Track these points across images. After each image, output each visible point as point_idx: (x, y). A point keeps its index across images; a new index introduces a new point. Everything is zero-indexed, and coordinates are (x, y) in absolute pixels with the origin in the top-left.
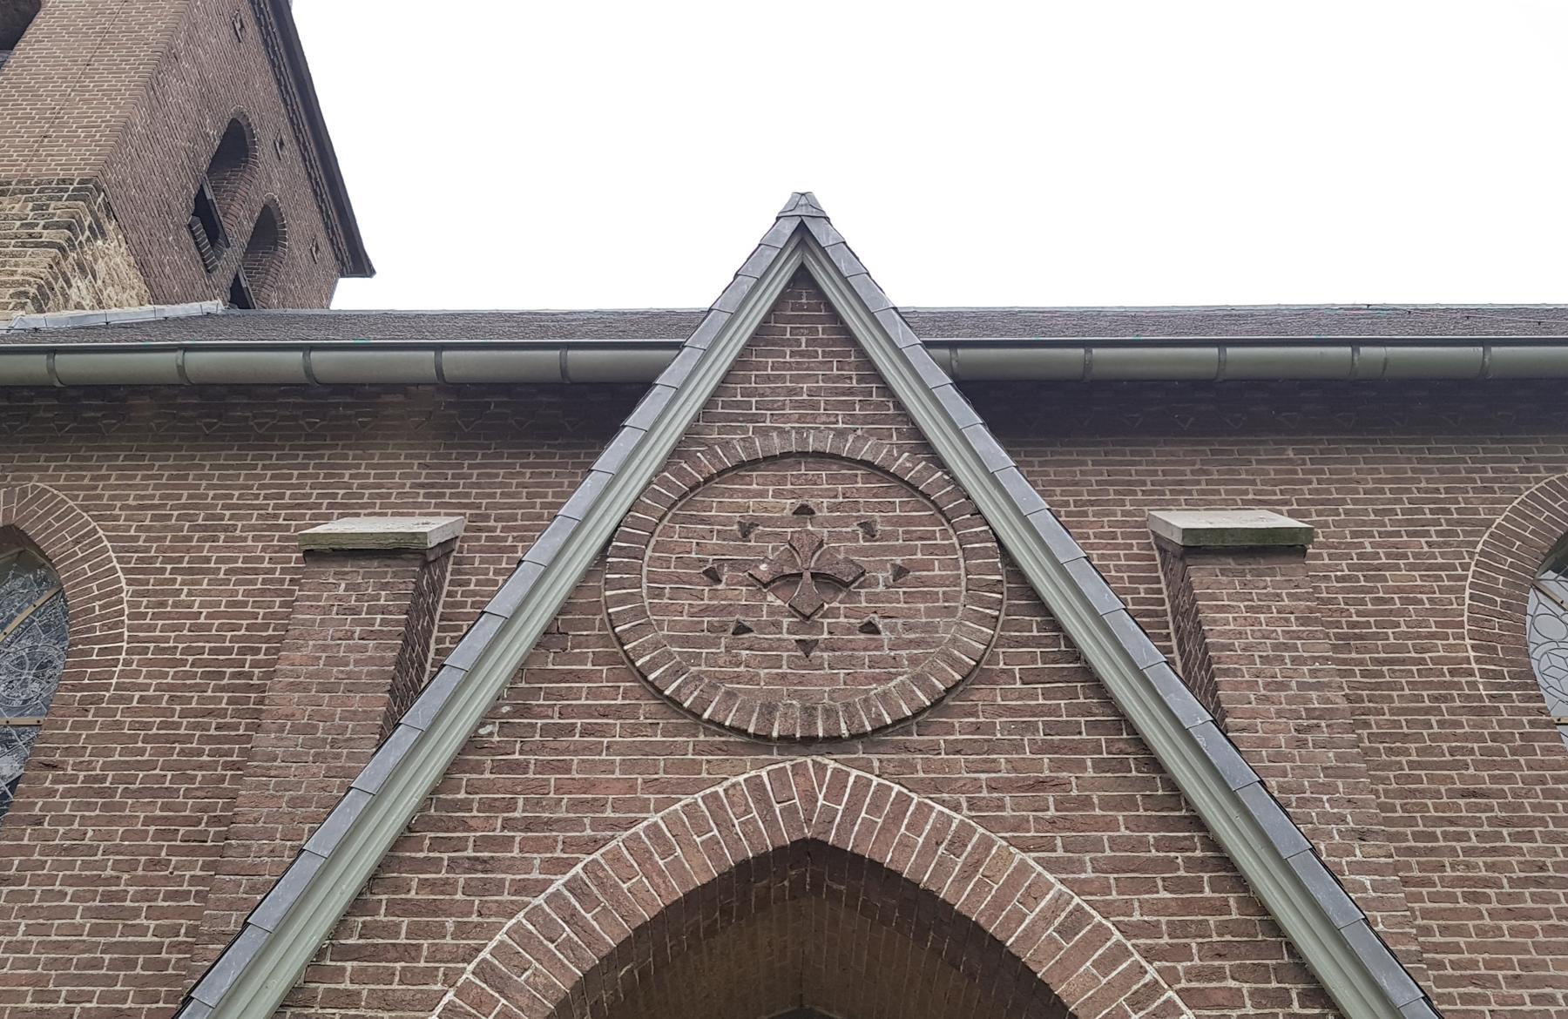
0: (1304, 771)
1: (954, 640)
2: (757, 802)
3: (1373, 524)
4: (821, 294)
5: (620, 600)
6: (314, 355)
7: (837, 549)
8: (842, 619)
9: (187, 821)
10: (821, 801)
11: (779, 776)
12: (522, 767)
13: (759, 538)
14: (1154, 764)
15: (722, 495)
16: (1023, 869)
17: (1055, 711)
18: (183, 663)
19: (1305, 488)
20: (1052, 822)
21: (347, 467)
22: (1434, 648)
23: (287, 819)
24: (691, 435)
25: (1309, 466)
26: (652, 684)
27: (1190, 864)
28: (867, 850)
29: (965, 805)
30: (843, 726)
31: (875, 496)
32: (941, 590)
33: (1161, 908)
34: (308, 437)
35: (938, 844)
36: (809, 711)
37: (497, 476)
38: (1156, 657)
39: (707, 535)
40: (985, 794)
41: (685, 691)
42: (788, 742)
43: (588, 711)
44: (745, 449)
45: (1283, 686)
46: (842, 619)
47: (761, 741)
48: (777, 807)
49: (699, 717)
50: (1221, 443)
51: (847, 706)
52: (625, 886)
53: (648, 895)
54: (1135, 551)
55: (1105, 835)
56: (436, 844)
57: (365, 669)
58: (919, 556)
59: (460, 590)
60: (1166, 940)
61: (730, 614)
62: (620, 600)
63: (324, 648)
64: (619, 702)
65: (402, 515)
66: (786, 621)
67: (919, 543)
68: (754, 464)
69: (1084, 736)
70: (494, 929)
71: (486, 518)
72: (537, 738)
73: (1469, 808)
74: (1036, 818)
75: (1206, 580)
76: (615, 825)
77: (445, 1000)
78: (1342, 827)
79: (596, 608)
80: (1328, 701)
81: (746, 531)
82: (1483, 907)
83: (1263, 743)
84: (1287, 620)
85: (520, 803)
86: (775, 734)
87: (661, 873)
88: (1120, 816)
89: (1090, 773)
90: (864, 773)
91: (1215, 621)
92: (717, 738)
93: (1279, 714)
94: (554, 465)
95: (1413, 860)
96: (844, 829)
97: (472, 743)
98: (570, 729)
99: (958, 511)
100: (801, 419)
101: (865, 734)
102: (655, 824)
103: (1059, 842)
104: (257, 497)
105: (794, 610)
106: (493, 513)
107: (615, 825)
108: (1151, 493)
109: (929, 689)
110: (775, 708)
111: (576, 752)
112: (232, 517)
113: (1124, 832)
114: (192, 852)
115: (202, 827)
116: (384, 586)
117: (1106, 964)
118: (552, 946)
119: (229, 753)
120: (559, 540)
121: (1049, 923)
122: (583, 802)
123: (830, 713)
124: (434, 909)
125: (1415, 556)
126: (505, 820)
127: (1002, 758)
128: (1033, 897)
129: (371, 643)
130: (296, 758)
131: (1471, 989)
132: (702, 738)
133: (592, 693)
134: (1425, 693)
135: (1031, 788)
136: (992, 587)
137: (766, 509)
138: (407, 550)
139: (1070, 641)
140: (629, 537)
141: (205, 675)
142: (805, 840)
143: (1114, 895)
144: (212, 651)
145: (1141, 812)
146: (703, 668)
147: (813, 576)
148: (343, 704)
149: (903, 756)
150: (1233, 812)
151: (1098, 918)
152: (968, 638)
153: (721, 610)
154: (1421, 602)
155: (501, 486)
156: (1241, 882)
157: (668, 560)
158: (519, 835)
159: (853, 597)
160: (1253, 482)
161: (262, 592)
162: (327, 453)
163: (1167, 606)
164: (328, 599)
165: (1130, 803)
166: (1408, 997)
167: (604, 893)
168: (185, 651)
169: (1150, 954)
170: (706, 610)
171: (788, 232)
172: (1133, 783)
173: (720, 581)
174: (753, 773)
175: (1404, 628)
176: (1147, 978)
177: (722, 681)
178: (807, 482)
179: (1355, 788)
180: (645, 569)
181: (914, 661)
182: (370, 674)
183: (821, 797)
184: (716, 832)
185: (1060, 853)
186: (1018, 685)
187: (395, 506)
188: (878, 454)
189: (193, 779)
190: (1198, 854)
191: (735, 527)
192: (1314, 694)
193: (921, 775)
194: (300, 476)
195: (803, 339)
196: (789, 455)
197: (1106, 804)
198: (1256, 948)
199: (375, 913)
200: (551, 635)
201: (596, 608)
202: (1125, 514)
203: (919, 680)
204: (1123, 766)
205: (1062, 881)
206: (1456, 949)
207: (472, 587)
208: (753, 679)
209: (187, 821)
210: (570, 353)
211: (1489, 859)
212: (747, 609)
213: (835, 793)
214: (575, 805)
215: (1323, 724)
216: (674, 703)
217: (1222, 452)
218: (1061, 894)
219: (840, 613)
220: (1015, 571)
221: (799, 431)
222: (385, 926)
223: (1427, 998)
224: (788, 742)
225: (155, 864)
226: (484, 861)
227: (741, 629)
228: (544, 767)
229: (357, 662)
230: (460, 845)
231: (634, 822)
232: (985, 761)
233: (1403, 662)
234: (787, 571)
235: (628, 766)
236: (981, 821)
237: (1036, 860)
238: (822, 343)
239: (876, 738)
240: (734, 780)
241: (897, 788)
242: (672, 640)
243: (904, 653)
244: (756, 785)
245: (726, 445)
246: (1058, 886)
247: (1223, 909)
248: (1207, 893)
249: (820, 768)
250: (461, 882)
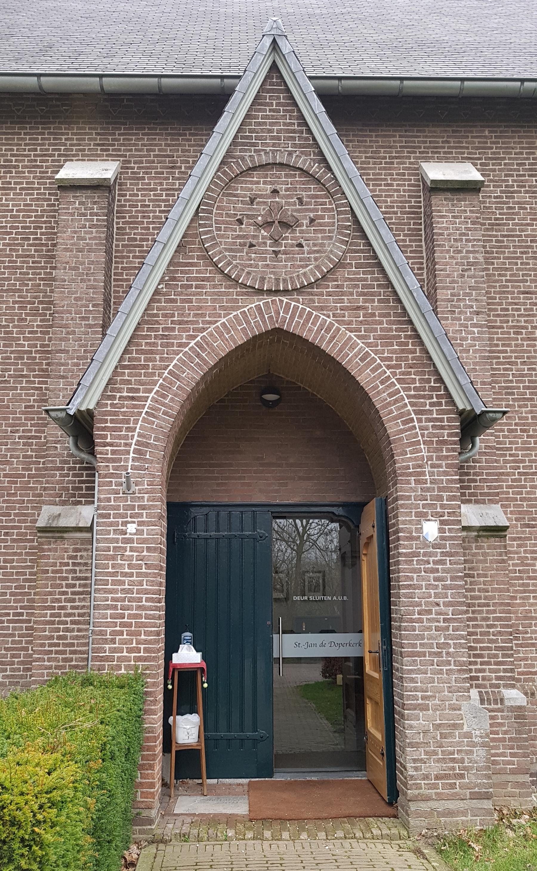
0: (462, 288)
1: (331, 251)
2: (259, 314)
3: (515, 170)
4: (281, 77)
5: (206, 233)
6: (43, 79)
7: (288, 209)
8: (290, 241)
9: (30, 303)
10: (281, 314)
11: (266, 304)
12: (175, 301)
13: (258, 203)
14: (399, 301)
15: (242, 183)
16: (350, 338)
17: (366, 280)
18: (11, 233)
19: (490, 151)
20: (361, 322)
21: (63, 134)
22: (527, 230)
23: (75, 306)
24: (229, 154)
25: (493, 140)
26: (220, 268)
27: (406, 337)
28: (297, 332)
29: (331, 316)
30: (290, 286)
31: (303, 184)
32: (327, 228)
33: (394, 352)
34: (42, 117)
35: (321, 330)
36: (277, 280)
37: (132, 140)
38: (404, 261)
39: (237, 202)
40: (339, 311)
41: (232, 272)
42: (270, 292)
43: (196, 279)
44: (251, 161)
45: (460, 252)
46: (290, 241)
47: (260, 291)
48: (266, 316)
49: (238, 282)
50: (457, 126)
51: (291, 278)
52: (215, 345)
53: (223, 348)
54: (413, 182)
55: (379, 327)
56: (149, 330)
57: (94, 242)
58: (320, 213)
59: (123, 198)
60: (394, 362)
61: (247, 238)
62: (206, 233)
63: (75, 232)
64: (208, 275)
65: (92, 160)
66: (269, 242)
67: (320, 207)
68: (254, 168)
69: (376, 290)
70: (172, 360)
71: (129, 162)
72: (179, 290)
73: (524, 298)
74: (356, 321)
75: (438, 203)
76: (210, 323)
77: (159, 382)
78: (471, 310)
79: (196, 235)
80: (476, 258)
81: (252, 201)
82: (519, 337)
83: (448, 276)
84: (467, 222)
85: (176, 315)
86: (265, 289)
87: (227, 340)
88: (385, 320)
89: (376, 304)
90: (297, 303)
91: (438, 223)
92: (244, 290)
93: (457, 264)
94: (157, 134)
95: (498, 319)
96: (290, 324)
97: (157, 292)
98: (191, 286)
99: (336, 193)
100: (274, 145)
101: (297, 289)
102: (224, 322)
103: (363, 329)
104: (25, 150)
105: (271, 238)
106: (132, 159)
107: (210, 323)
108: (423, 152)
109: (321, 271)
110: (265, 278)
111: (194, 295)
112: (16, 161)
113: (385, 325)
114: (35, 315)
115: (36, 305)
116: (95, 203)
117: (374, 370)
118: (192, 365)
119: (40, 274)
120: (181, 208)
121: (357, 357)
122: (198, 314)
123: (285, 281)
124: (151, 352)
125: (530, 186)
126: (171, 321)
127: (346, 298)
128: (352, 348)
129: (94, 230)
130: (73, 280)
131: (508, 366)
132: (239, 290)
133: (198, 272)
134: (518, 250)
135: (355, 309)
136: (347, 227)
137: (260, 190)
138: (102, 186)
139: (374, 252)
140: (207, 204)
141: (22, 239)
142: (276, 328)
143: (379, 348)
144: (22, 228)
145: (392, 318)
146: (238, 261)
147: (279, 222)
148: (88, 258)
149: (311, 297)
150: (422, 320)
151: (373, 355)
152: (336, 249)
153: (243, 237)
154: (526, 209)
155: (135, 145)
156: (422, 343)
157: (222, 214)
158: (177, 327)
159: (294, 231)
160: (467, 148)
161: (38, 199)
162: (52, 126)
163: (422, 209)
164: (72, 209)
165: (389, 315)
166: (466, 382)
167: (208, 347)
168: (11, 228)
169: (388, 367)
170: (238, 237)
171: (268, 45)
172: (391, 308)
173: (242, 224)
174: (258, 303)
175: (517, 221)
176: (387, 375)
177: (245, 267)
178: (277, 177)
179: (479, 295)
180: (214, 218)
181: (316, 259)
182: (96, 244)
183: (281, 312)
184: (245, 325)
185: (363, 333)
186: (354, 269)
187: (87, 156)
188: (305, 164)
189: (27, 285)
190: (409, 333)
191: (248, 199)
192: (471, 255)
193: (317, 304)
194: (42, 139)
195: (274, 102)
196: (269, 164)
197: (380, 315)
198: (424, 365)
199: (132, 353)
200: (181, 247)
201: (196, 235)
202: (410, 163)
203: (317, 267)
204: (388, 301)
205: (363, 343)
206: (506, 352)
207: (128, 197)
208: (257, 266)
209: (30, 303)
210: (162, 79)
211: (526, 319)
212: (254, 237)
213: (286, 311)
214: (195, 315)
215: (472, 268)
216: (228, 276)
217: (457, 131)
218: (362, 347)
219: (289, 238)
220: (356, 221)
221: (273, 152)
222: (136, 358)
223: (471, 382)
224: (270, 292)
225: (21, 320)
226: (166, 336)
227: (252, 245)
228: (183, 301)
229: (90, 239)
230: (157, 330)
231: (216, 322)
232: (340, 299)
233: (513, 236)
234: (269, 220)
235: (214, 301)
236: (337, 321)
237: (355, 335)
238: (283, 105)
239: (301, 290)
240: (250, 306)
241: (308, 309)
242: (226, 250)
243: (312, 256)
244: (258, 308)
245: (243, 159)
246: (361, 344)
247: (414, 352)
248: (410, 347)
249: (281, 301)
250: (159, 343)
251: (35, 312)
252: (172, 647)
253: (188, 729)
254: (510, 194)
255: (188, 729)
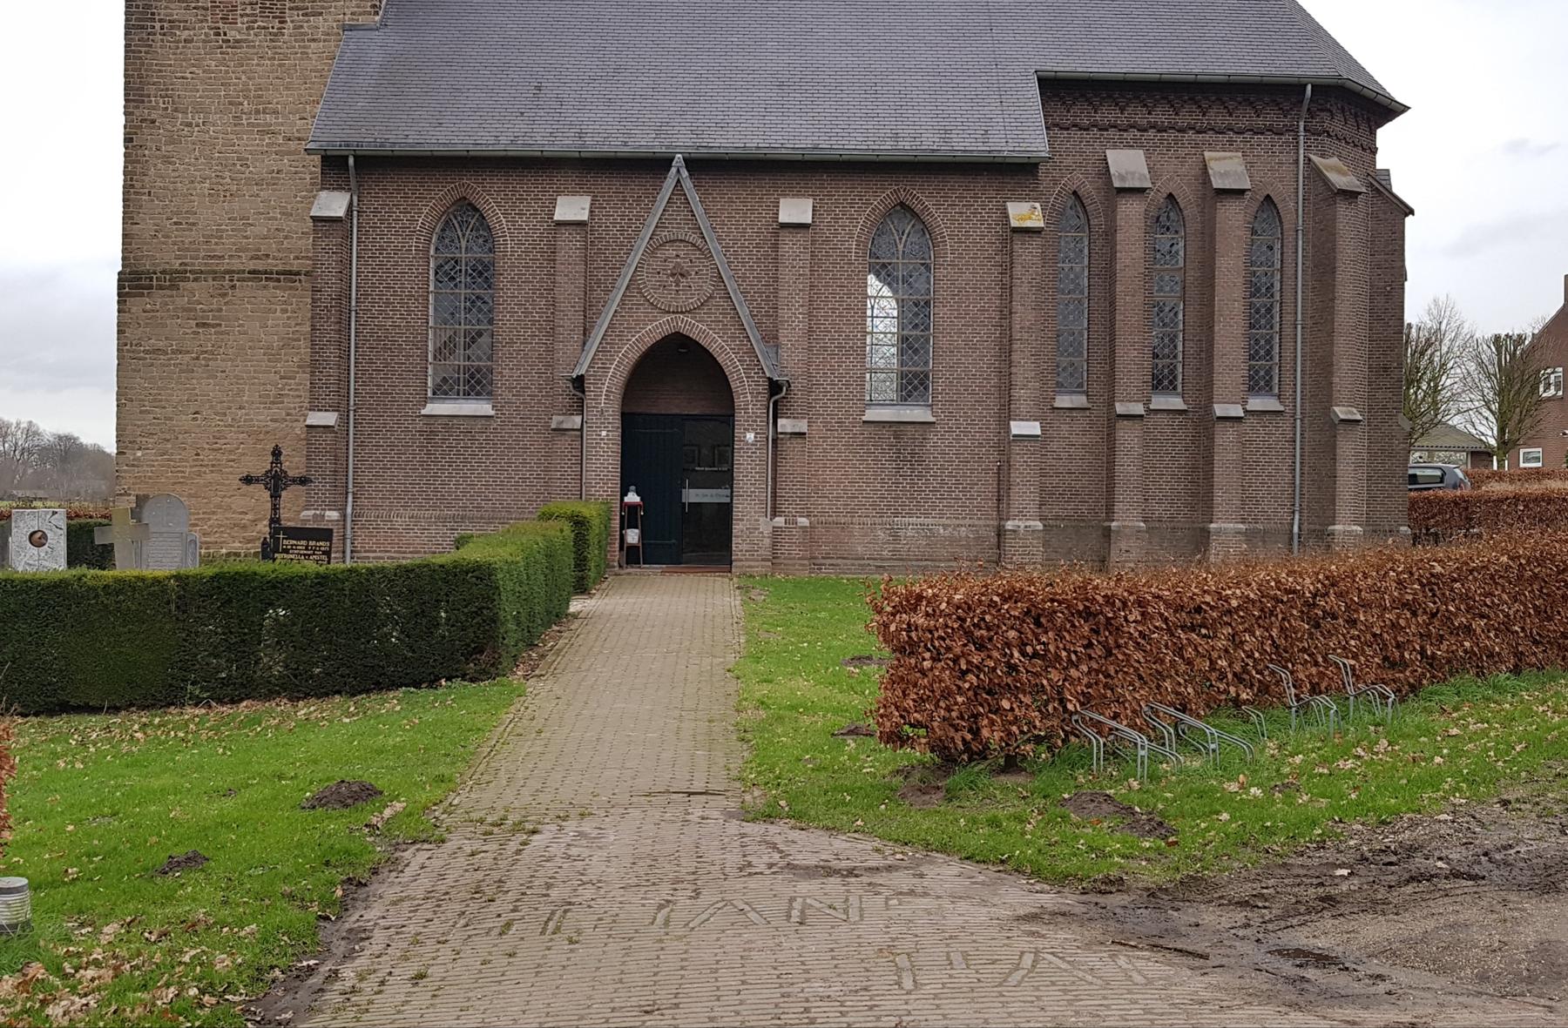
53: (649, 341)
251: (541, 296)
252: (624, 493)
253: (633, 536)
254: (836, 219)
255: (633, 536)
